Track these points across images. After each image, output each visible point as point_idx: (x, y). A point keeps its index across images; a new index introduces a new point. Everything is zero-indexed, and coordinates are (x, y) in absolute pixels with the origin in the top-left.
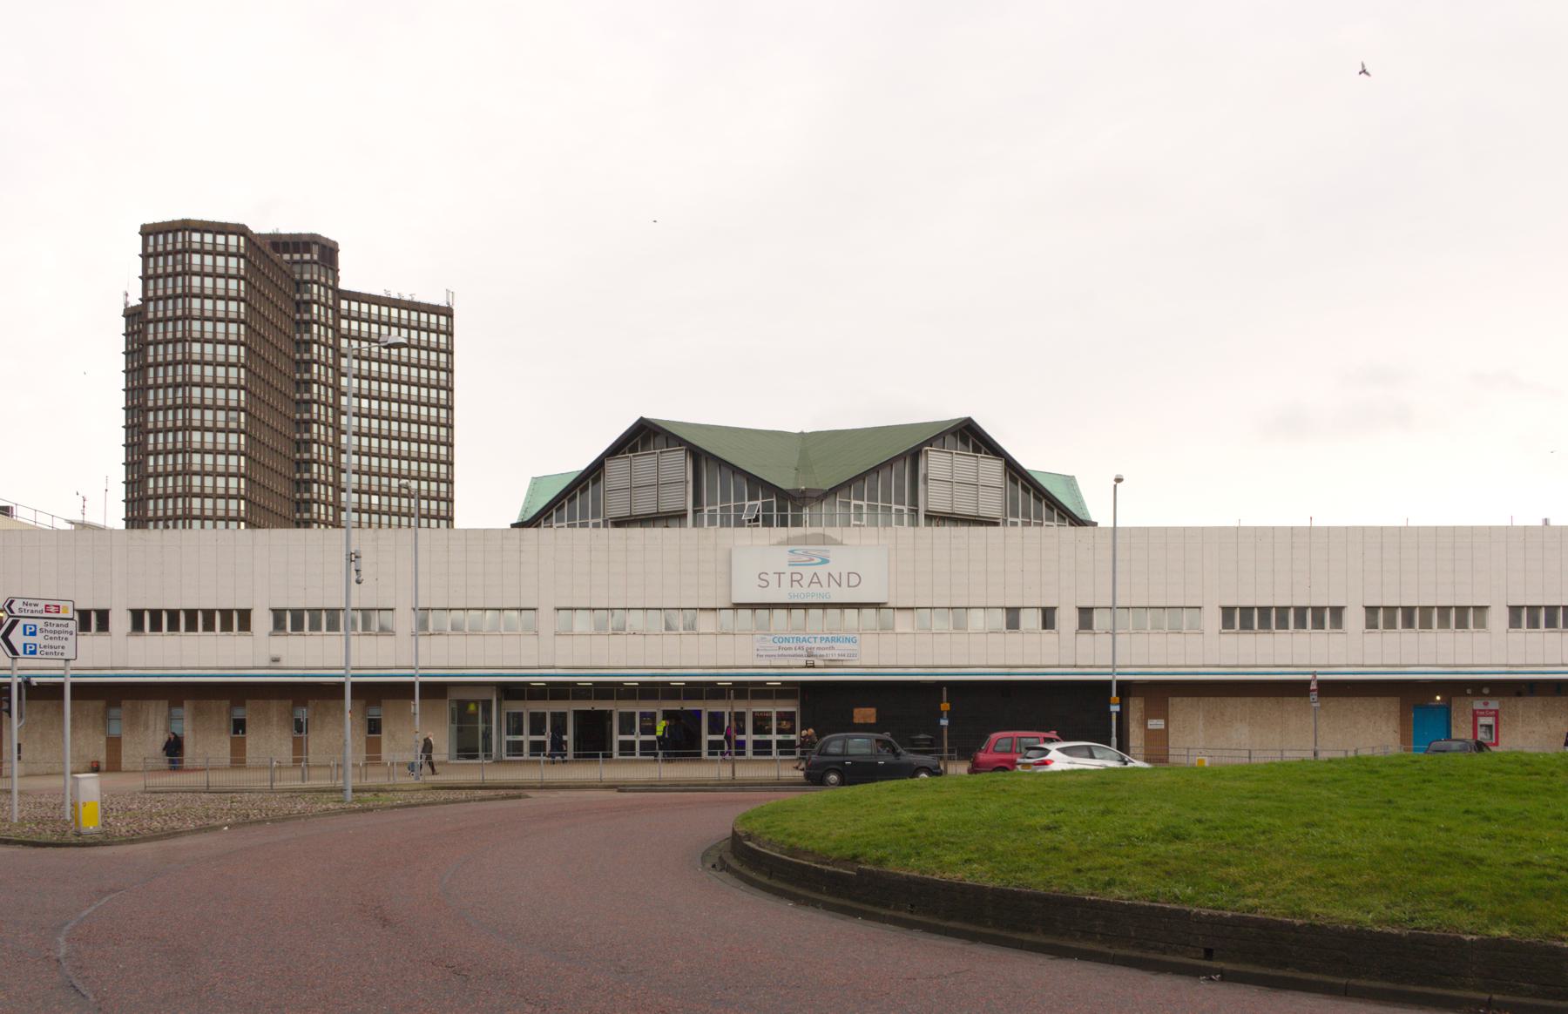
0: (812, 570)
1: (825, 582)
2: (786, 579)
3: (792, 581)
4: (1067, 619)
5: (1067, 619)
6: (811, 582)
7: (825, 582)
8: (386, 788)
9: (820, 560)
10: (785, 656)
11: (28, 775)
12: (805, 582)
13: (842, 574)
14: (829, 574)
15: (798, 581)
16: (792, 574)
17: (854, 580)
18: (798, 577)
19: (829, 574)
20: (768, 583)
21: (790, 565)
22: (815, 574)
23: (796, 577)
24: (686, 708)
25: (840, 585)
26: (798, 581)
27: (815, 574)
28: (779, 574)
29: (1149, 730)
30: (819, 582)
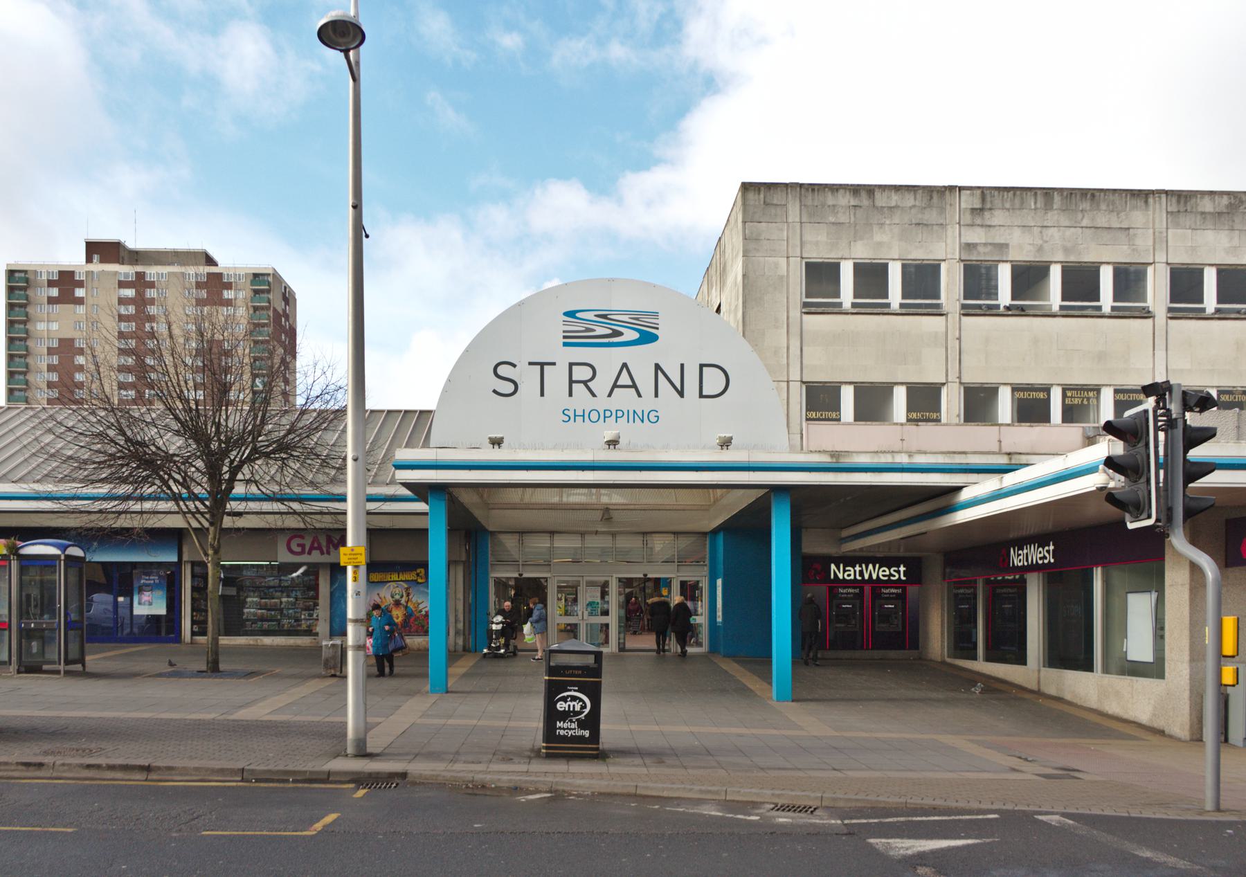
0: (618, 355)
1: (646, 384)
2: (556, 378)
3: (571, 382)
4: (951, 402)
5: (951, 402)
6: (615, 386)
7: (646, 384)
8: (24, 768)
9: (635, 335)
10: (619, 510)
11: (649, 562)
12: (602, 384)
13: (657, 330)
14: (658, 367)
15: (585, 383)
16: (571, 365)
17: (713, 381)
18: (584, 373)
19: (658, 367)
20: (563, 412)
21: (565, 344)
22: (625, 365)
23: (581, 373)
24: (525, 575)
25: (681, 394)
26: (585, 383)
27: (625, 365)
28: (542, 365)
29: (1189, 461)
30: (634, 386)
